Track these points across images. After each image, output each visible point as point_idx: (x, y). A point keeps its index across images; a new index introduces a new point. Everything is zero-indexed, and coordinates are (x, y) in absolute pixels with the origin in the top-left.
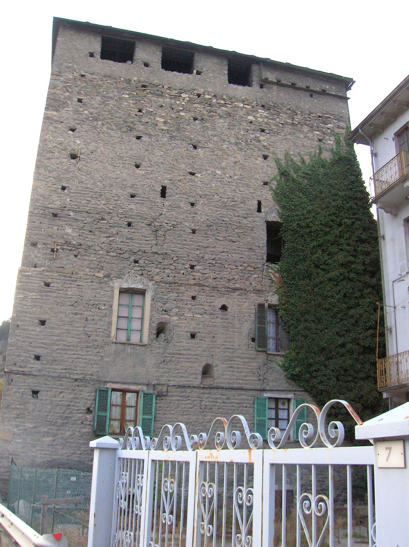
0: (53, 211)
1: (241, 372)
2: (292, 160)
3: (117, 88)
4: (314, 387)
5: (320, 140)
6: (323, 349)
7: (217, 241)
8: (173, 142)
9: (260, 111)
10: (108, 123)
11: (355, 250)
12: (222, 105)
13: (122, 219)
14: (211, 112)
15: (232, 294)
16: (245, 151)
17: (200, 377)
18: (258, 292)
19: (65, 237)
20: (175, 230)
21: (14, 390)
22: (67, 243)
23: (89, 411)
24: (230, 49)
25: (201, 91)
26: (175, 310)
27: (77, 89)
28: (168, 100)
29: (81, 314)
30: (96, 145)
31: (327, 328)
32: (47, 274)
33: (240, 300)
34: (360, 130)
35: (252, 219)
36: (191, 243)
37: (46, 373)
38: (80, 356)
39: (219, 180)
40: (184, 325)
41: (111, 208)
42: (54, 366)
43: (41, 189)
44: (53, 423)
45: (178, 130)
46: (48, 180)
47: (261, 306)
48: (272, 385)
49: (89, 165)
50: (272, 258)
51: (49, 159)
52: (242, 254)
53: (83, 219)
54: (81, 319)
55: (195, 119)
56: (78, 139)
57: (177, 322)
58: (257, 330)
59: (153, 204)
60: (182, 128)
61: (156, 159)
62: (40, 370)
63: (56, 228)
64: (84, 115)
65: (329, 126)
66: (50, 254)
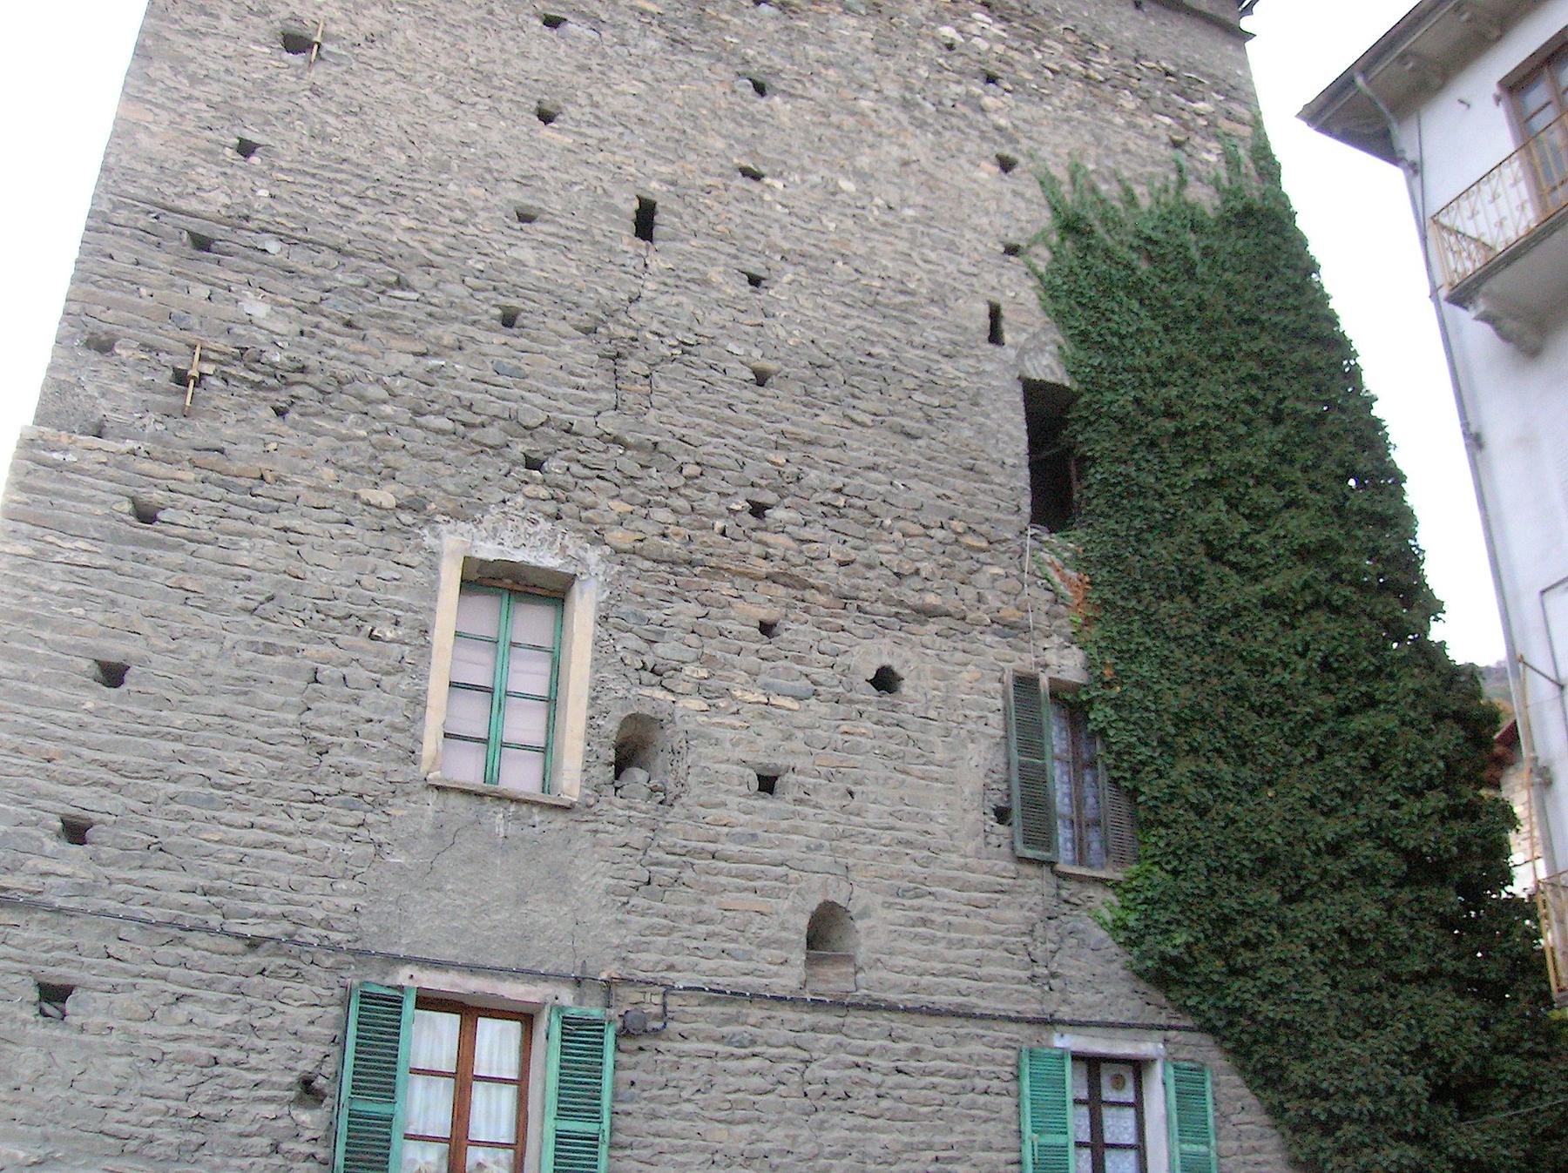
0: (194, 225)
1: (962, 944)
2: (1094, 190)
4: (1240, 1011)
5: (1176, 145)
7: (847, 424)
9: (978, 16)
13: (480, 296)
15: (914, 627)
17: (798, 956)
18: (1010, 629)
20: (691, 365)
23: (308, 1091)
26: (694, 671)
29: (292, 652)
31: (1270, 784)
32: (147, 466)
33: (946, 656)
34: (1360, 81)
35: (972, 362)
37: (112, 905)
39: (849, 211)
40: (730, 734)
43: (152, 135)
44: (132, 1145)
47: (1025, 683)
48: (1083, 1002)
49: (355, 82)
51: (192, 33)
54: (290, 672)
57: (701, 719)
58: (1015, 779)
59: (605, 256)
62: (83, 889)
63: (204, 291)
65: (1200, 106)
66: (168, 392)
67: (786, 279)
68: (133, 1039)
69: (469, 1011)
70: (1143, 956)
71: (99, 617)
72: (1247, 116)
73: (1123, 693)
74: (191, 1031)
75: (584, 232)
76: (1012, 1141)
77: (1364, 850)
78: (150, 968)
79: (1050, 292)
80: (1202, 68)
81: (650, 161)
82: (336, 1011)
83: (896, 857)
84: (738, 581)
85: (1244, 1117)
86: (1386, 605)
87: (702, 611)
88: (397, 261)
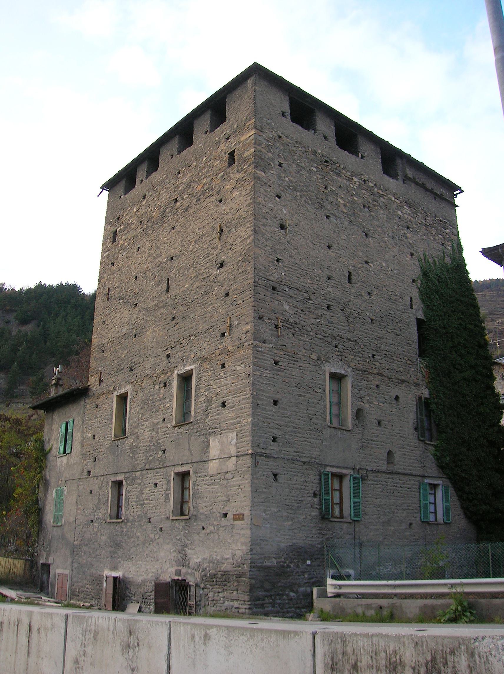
0: (272, 283)
2: (428, 261)
3: (308, 158)
5: (443, 244)
9: (405, 207)
13: (324, 301)
15: (401, 385)
16: (399, 247)
17: (386, 463)
18: (417, 385)
19: (284, 313)
21: (260, 472)
22: (286, 320)
26: (367, 398)
28: (344, 181)
29: (304, 396)
30: (298, 218)
32: (276, 351)
34: (500, 250)
35: (407, 314)
37: (282, 456)
41: (315, 288)
47: (420, 398)
50: (422, 353)
51: (264, 225)
52: (403, 348)
53: (296, 296)
56: (284, 208)
62: (278, 453)
65: (447, 231)
67: (375, 293)
71: (272, 389)
72: (456, 233)
75: (340, 282)
76: (418, 502)
78: (290, 469)
80: (448, 218)
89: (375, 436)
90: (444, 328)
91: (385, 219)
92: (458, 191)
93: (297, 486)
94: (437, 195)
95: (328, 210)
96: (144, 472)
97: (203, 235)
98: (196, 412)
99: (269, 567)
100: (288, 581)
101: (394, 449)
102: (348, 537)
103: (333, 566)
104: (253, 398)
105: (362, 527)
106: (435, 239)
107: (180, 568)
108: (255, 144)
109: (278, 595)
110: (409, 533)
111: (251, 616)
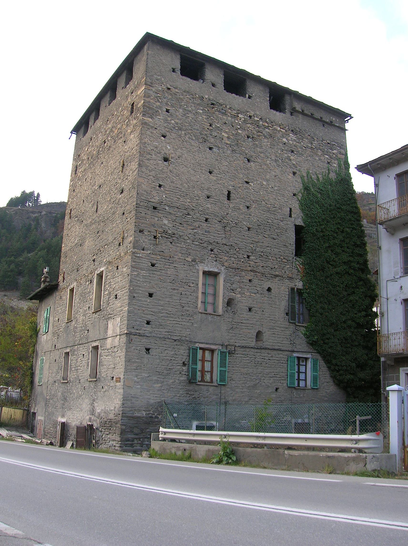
0: (154, 205)
1: (280, 338)
2: (311, 178)
3: (194, 103)
4: (325, 350)
5: (328, 163)
6: (332, 324)
7: (264, 238)
8: (234, 155)
9: (291, 135)
10: (189, 133)
11: (352, 252)
12: (267, 127)
13: (202, 216)
14: (259, 132)
15: (274, 279)
17: (254, 340)
18: (290, 279)
19: (163, 227)
20: (237, 227)
21: (134, 347)
22: (165, 232)
23: (184, 364)
24: (273, 80)
25: (252, 113)
26: (239, 290)
27: (165, 100)
29: (178, 290)
31: (334, 309)
32: (153, 256)
33: (279, 284)
34: (369, 166)
35: (286, 222)
36: (247, 238)
37: (155, 335)
38: (177, 322)
39: (265, 189)
40: (244, 301)
41: (194, 205)
42: (161, 330)
43: (145, 185)
44: (161, 373)
45: (237, 145)
46: (149, 178)
47: (292, 289)
48: (298, 348)
49: (177, 168)
50: (298, 252)
51: (148, 159)
52: (280, 249)
53: (175, 213)
54: (178, 293)
55: (248, 137)
56: (168, 145)
57: (240, 298)
58: (290, 308)
59: (222, 205)
60: (240, 143)
61: (223, 168)
62: (151, 333)
63: (157, 219)
64: (171, 124)
65: (334, 151)
66: (153, 240)
68: (160, 356)
69: (204, 349)
70: (310, 340)
71: (148, 285)
72: (344, 153)
73: (309, 291)
74: (168, 355)
76: (286, 372)
77: (350, 322)
78: (161, 345)
79: (301, 204)
80: (336, 141)
81: (229, 181)
82: (188, 351)
83: (270, 322)
84: (246, 272)
85: (324, 368)
86: (359, 273)
87: (240, 278)
88: (188, 210)
89: (245, 320)
90: (322, 232)
91: (269, 146)
92: (349, 118)
93: (167, 357)
94: (327, 123)
95: (212, 143)
96: (79, 346)
97: (115, 169)
98: (103, 303)
99: (139, 417)
100: (156, 428)
101: (264, 330)
102: (215, 397)
103: (198, 419)
104: (130, 292)
105: (228, 389)
106: (320, 159)
107: (91, 416)
108: (144, 97)
109: (146, 438)
110: (275, 396)
111: (121, 452)
